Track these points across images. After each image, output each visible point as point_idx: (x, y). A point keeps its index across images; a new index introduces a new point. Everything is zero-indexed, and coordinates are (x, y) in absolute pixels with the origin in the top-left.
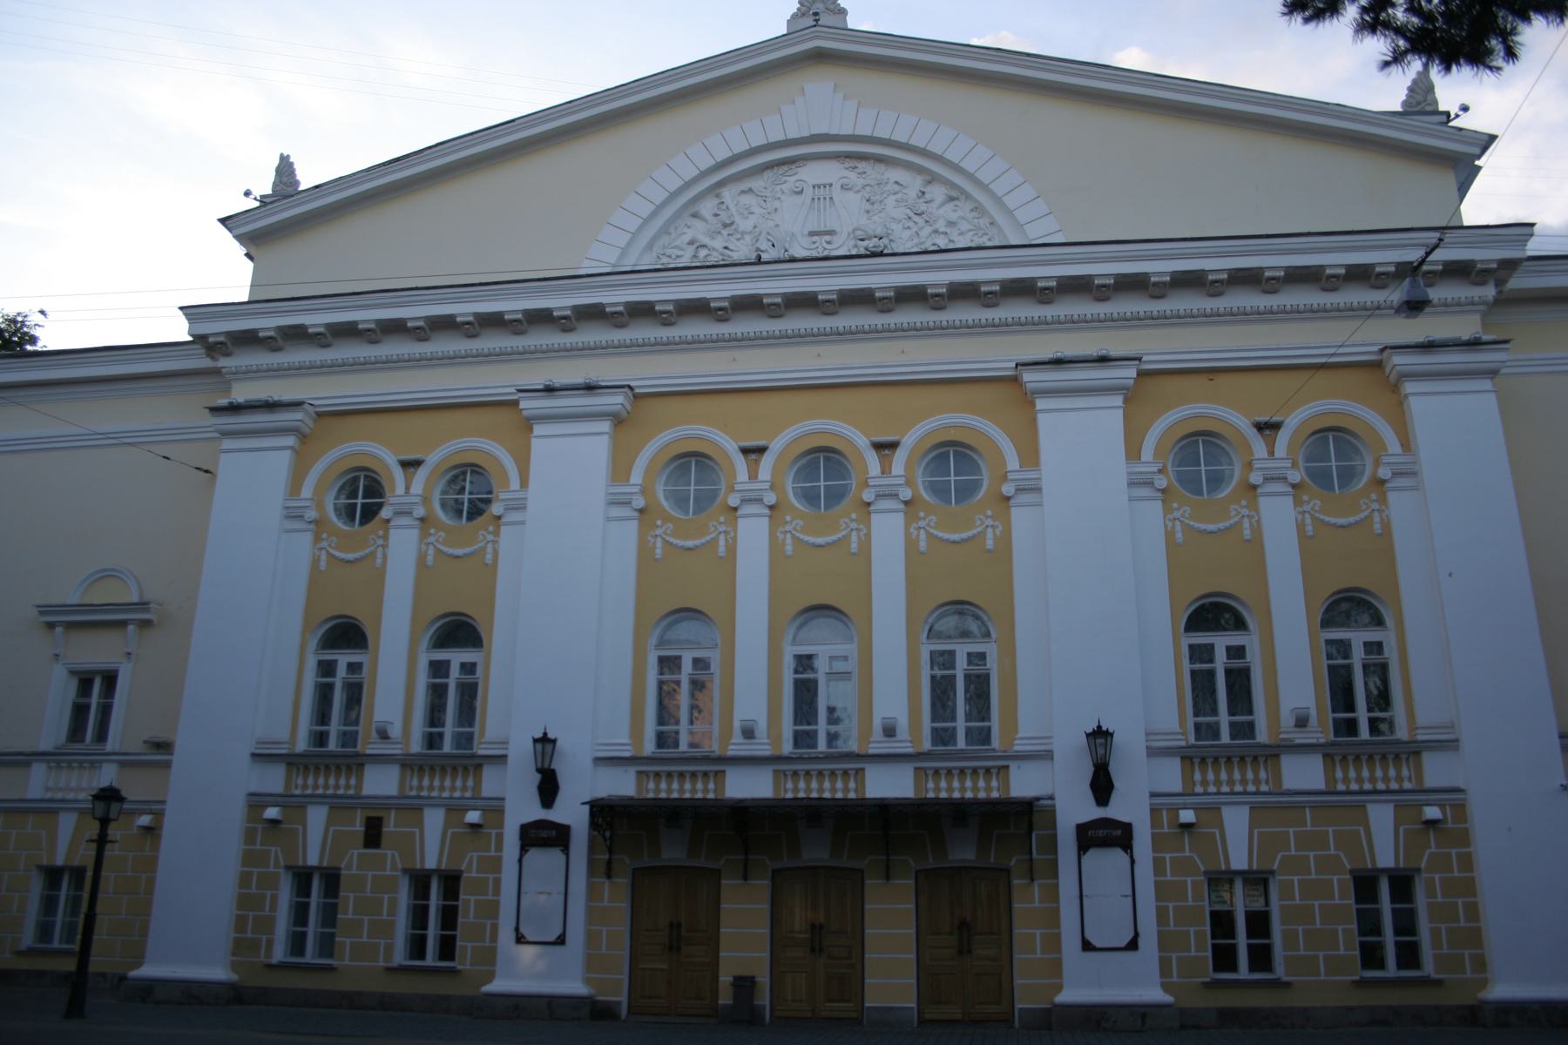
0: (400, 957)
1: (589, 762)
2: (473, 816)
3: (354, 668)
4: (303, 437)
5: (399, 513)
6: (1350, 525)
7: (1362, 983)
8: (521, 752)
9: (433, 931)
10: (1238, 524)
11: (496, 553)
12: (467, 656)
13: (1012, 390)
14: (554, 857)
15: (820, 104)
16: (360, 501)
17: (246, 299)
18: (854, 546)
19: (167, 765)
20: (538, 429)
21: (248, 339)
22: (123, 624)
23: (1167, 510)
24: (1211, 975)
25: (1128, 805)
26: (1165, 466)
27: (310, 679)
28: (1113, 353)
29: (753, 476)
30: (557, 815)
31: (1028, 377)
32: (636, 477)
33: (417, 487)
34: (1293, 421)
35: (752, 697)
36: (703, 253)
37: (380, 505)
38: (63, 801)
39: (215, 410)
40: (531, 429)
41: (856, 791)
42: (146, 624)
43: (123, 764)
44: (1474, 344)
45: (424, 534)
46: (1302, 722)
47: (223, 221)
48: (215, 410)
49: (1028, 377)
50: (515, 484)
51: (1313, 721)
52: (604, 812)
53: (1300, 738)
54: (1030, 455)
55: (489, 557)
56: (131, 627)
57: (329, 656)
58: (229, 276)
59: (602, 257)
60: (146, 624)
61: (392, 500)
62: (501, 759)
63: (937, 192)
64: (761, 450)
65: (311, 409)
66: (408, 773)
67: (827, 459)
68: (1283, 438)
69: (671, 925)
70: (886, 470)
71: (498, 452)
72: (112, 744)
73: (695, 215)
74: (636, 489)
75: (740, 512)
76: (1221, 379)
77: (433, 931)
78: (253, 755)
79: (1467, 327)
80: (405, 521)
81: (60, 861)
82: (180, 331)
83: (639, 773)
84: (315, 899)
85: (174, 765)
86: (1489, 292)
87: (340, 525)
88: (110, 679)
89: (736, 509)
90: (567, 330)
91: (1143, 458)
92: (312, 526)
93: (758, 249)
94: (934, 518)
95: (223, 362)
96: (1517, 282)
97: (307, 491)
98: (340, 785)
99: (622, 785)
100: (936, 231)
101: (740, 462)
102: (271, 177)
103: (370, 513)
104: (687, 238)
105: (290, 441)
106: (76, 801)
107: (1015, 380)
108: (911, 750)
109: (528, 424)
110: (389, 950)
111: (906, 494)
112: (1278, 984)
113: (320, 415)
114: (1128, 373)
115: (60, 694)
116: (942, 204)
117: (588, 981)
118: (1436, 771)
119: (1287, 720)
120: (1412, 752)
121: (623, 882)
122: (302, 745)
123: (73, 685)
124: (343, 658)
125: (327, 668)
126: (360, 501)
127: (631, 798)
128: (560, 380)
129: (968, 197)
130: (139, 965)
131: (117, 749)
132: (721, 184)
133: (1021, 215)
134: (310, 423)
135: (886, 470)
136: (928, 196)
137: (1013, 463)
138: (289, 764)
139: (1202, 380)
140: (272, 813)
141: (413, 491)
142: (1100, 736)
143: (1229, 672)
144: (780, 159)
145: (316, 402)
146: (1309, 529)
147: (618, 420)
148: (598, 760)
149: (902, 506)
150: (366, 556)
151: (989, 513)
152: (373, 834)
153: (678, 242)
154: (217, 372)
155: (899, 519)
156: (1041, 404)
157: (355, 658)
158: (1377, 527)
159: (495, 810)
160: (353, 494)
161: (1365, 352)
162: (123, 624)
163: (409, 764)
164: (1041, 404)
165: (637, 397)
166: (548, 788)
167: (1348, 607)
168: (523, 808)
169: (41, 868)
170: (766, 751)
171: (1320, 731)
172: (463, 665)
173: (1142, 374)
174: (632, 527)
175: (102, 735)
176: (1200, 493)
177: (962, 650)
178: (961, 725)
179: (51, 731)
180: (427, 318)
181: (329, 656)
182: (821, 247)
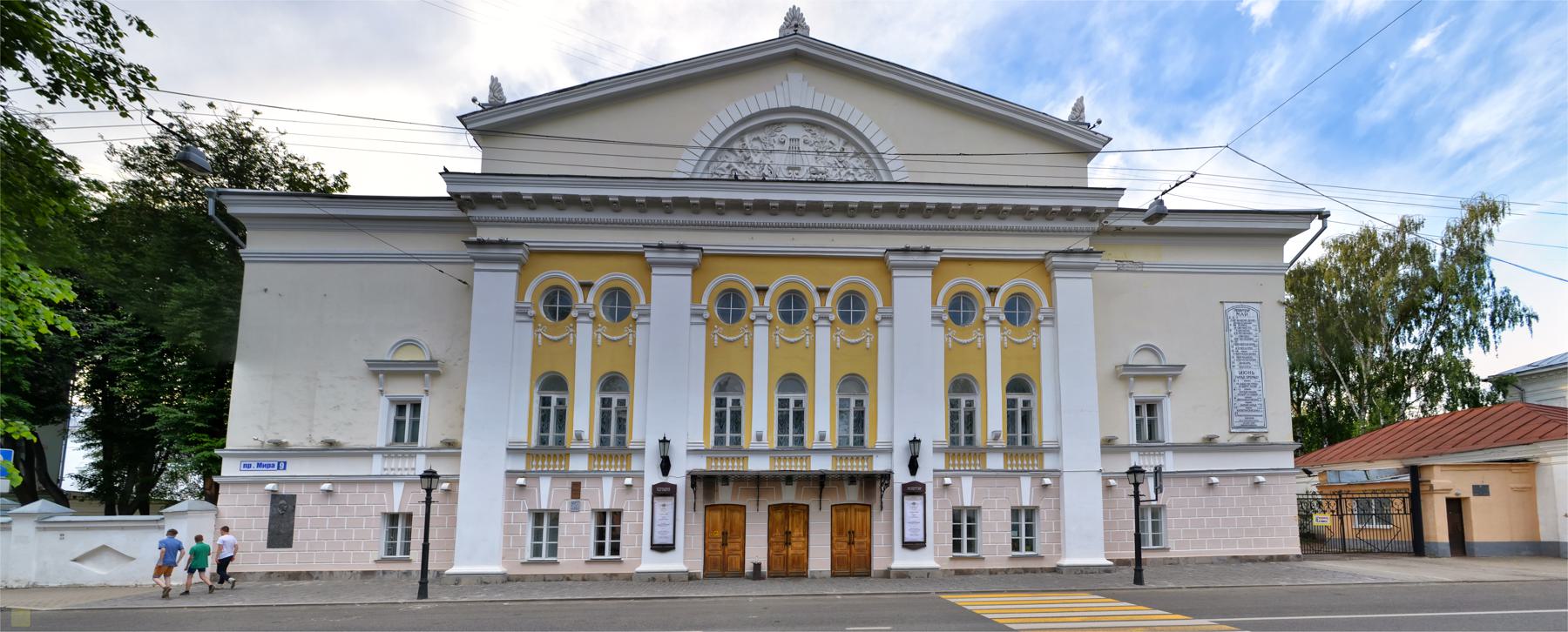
0: (528, 556)
2: (628, 481)
4: (523, 266)
5: (581, 314)
7: (1013, 558)
8: (652, 447)
9: (608, 541)
11: (751, 342)
13: (883, 265)
14: (669, 502)
15: (796, 89)
19: (459, 455)
21: (484, 200)
23: (946, 331)
24: (951, 554)
25: (678, 477)
28: (932, 247)
29: (762, 304)
30: (670, 480)
33: (590, 300)
34: (598, 283)
39: (468, 243)
43: (428, 455)
44: (1088, 252)
46: (996, 438)
48: (468, 243)
49: (892, 258)
50: (643, 301)
51: (828, 438)
52: (694, 478)
53: (996, 445)
54: (889, 301)
58: (468, 158)
59: (684, 169)
62: (642, 451)
63: (850, 149)
68: (830, 297)
70: (823, 304)
72: (422, 441)
76: (976, 267)
77: (608, 541)
79: (1084, 244)
81: (396, 510)
82: (440, 189)
84: (545, 527)
86: (1096, 226)
88: (416, 406)
90: (669, 212)
95: (470, 213)
96: (1114, 222)
97: (528, 299)
98: (557, 465)
99: (701, 464)
101: (755, 295)
103: (564, 314)
105: (516, 267)
107: (1042, 262)
109: (649, 267)
110: (587, 551)
111: (707, 315)
112: (1038, 557)
114: (696, 256)
117: (504, 564)
118: (1049, 462)
119: (990, 436)
120: (1040, 453)
121: (701, 511)
122: (534, 443)
128: (912, 245)
132: (743, 133)
133: (891, 166)
135: (823, 304)
137: (880, 305)
139: (964, 266)
140: (521, 481)
142: (915, 441)
143: (795, 413)
144: (772, 120)
147: (695, 268)
152: (576, 491)
154: (467, 220)
156: (895, 273)
157: (622, 397)
159: (639, 476)
160: (554, 302)
161: (1037, 254)
163: (593, 454)
164: (895, 273)
165: (704, 256)
166: (665, 466)
167: (1018, 385)
168: (653, 477)
169: (385, 514)
171: (1002, 442)
173: (942, 260)
175: (414, 438)
178: (791, 435)
181: (1012, 396)
182: (793, 175)
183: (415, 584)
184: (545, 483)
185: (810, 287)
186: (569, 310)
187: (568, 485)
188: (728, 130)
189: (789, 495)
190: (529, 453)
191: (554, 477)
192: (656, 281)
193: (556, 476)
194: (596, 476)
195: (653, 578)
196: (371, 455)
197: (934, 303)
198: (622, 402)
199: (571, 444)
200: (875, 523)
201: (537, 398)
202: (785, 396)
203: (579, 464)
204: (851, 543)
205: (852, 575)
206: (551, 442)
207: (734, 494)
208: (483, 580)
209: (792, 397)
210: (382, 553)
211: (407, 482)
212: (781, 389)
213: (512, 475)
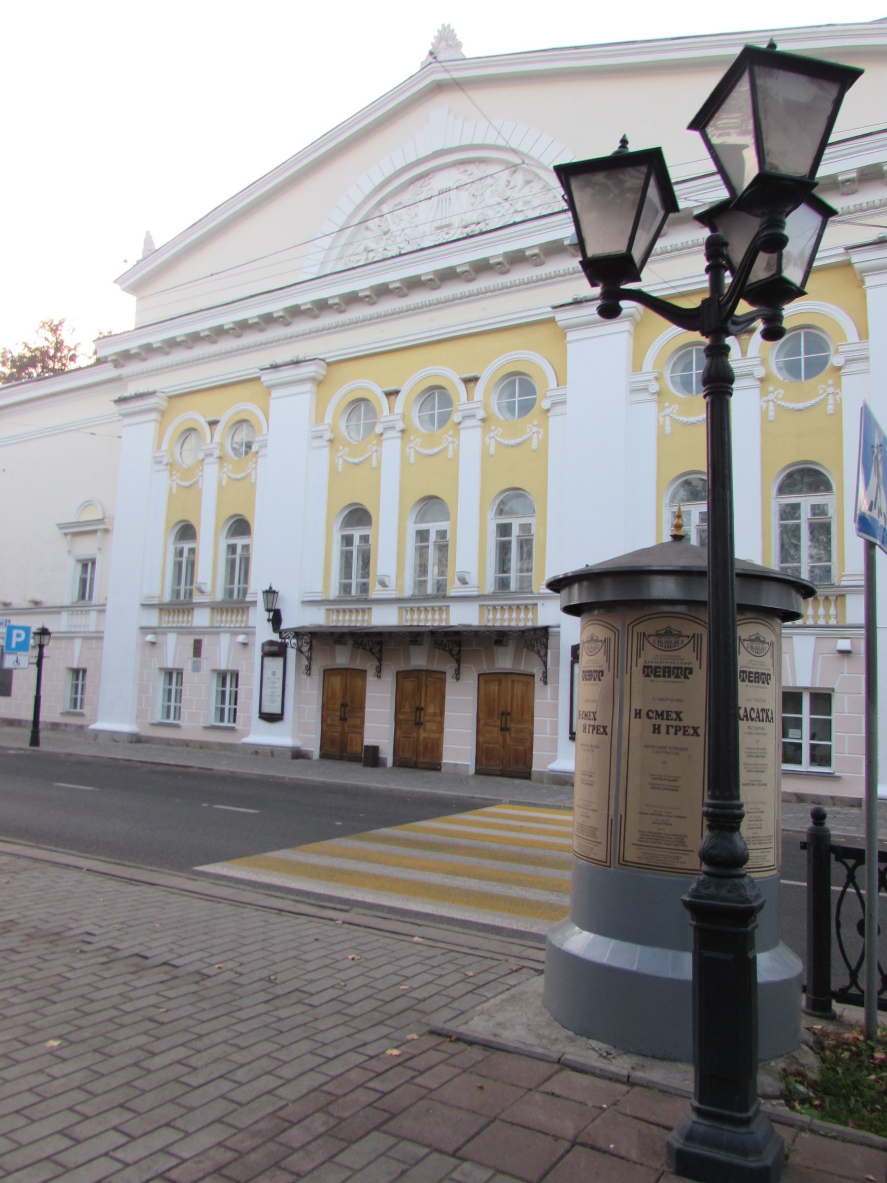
1: (137, 607)
3: (818, 510)
4: (163, 413)
6: (807, 408)
10: (446, 448)
11: (379, 462)
12: (364, 531)
15: (442, 125)
16: (517, 399)
17: (132, 327)
18: (534, 445)
20: (570, 336)
22: (95, 532)
26: (661, 374)
27: (337, 548)
28: (301, 357)
29: (470, 398)
31: (856, 258)
32: (328, 420)
33: (217, 438)
35: (471, 557)
36: (371, 255)
37: (450, 413)
38: (75, 632)
40: (565, 336)
41: (836, 617)
42: (106, 531)
45: (486, 431)
47: (114, 282)
49: (856, 258)
55: (374, 464)
56: (99, 534)
57: (348, 532)
60: (106, 531)
61: (382, 420)
64: (397, 393)
65: (163, 395)
66: (331, 614)
67: (521, 381)
69: (342, 705)
71: (253, 409)
73: (367, 229)
74: (398, 417)
75: (385, 436)
78: (143, 605)
80: (468, 423)
83: (480, 606)
85: (107, 612)
87: (680, 395)
89: (382, 435)
91: (644, 370)
92: (655, 397)
93: (399, 248)
94: (500, 429)
97: (165, 447)
99: (317, 618)
100: (516, 212)
102: (141, 247)
104: (362, 247)
105: (154, 416)
106: (80, 632)
108: (476, 593)
113: (171, 398)
115: (73, 573)
116: (522, 188)
123: (79, 567)
124: (357, 533)
125: (348, 540)
126: (517, 399)
127: (321, 626)
128: (279, 361)
129: (540, 178)
130: (95, 721)
131: (97, 603)
134: (165, 404)
136: (511, 185)
138: (161, 610)
141: (214, 440)
144: (417, 174)
145: (165, 390)
146: (771, 415)
147: (319, 383)
148: (304, 603)
149: (757, 383)
150: (367, 458)
151: (535, 423)
153: (358, 251)
155: (478, 432)
157: (192, 545)
158: (830, 408)
162: (95, 532)
163: (217, 608)
165: (329, 364)
168: (265, 633)
170: (392, 595)
172: (813, 507)
174: (326, 452)
176: (690, 392)
177: (516, 524)
179: (68, 593)
180: (540, 246)
181: (348, 532)
183: (28, 732)
184: (172, 639)
185: (452, 378)
186: (450, 414)
187: (189, 641)
188: (359, 207)
189: (419, 660)
190: (163, 608)
191: (179, 634)
192: (274, 405)
193: (182, 631)
194: (214, 631)
195: (257, 751)
196: (59, 613)
197: (637, 367)
198: (365, 539)
199: (376, 592)
200: (537, 701)
201: (171, 550)
202: (423, 526)
203: (201, 618)
204: (504, 729)
205: (502, 774)
206: (513, 586)
207: (353, 657)
208: (114, 737)
209: (433, 527)
210: (67, 706)
211: (84, 638)
212: (421, 517)
213: (145, 630)
